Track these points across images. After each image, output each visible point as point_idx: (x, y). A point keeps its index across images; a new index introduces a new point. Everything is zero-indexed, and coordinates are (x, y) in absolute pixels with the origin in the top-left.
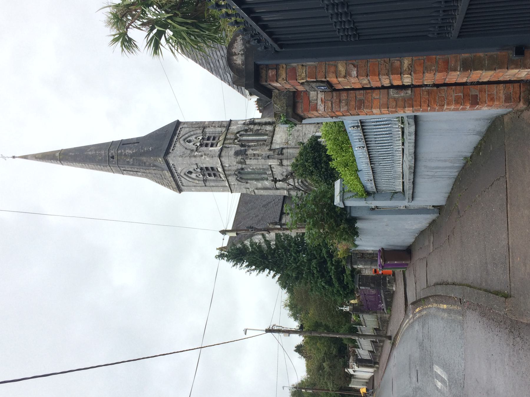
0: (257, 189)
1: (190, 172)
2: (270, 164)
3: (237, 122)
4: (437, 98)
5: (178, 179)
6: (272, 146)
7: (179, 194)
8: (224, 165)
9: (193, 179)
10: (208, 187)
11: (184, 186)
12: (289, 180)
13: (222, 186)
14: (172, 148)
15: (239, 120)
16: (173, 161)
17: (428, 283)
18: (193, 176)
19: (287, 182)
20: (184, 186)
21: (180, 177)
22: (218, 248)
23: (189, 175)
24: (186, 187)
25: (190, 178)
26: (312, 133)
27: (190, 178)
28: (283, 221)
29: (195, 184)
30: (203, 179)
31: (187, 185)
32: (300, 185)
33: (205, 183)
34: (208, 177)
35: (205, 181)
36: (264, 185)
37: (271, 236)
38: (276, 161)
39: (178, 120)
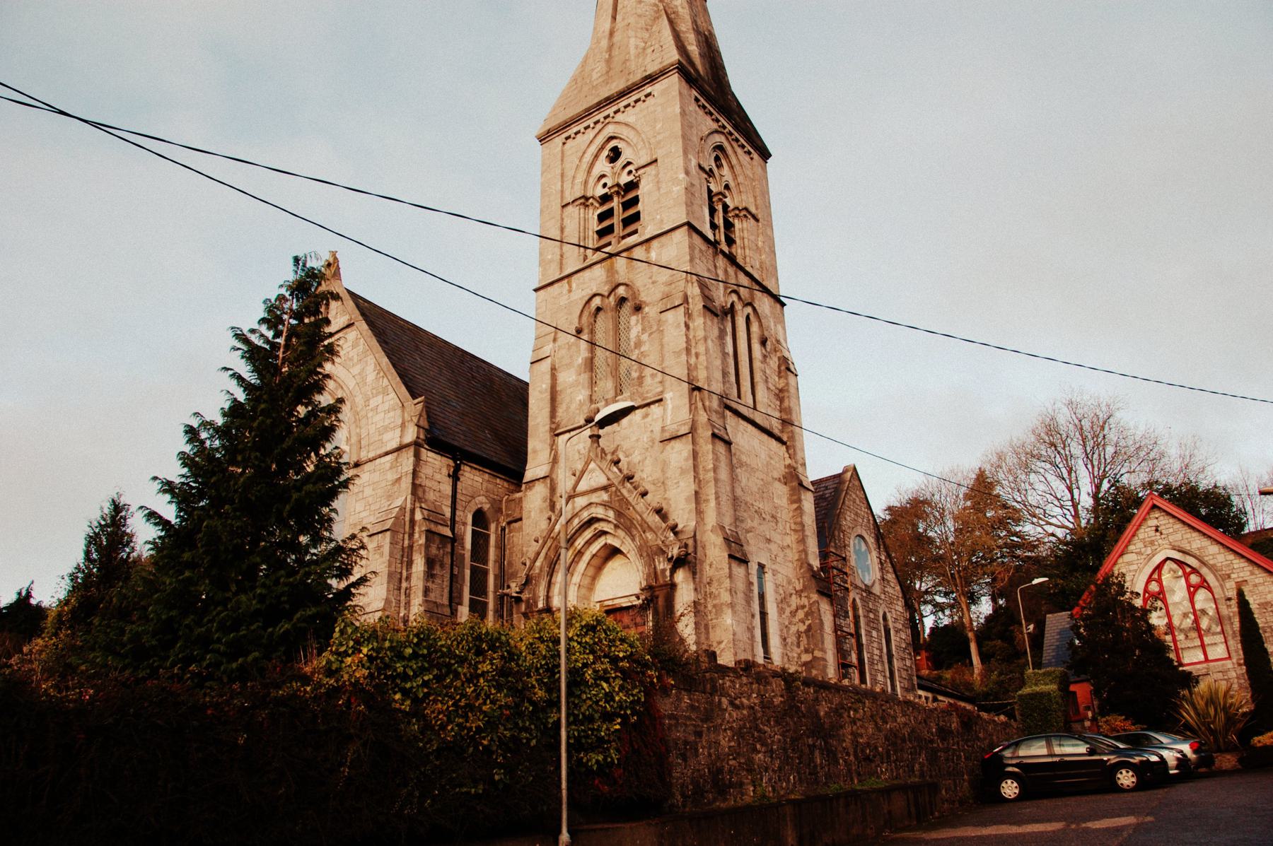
0: (553, 369)
1: (615, 154)
2: (668, 396)
3: (781, 320)
4: (340, 683)
5: (590, 122)
6: (690, 447)
7: (536, 134)
8: (655, 243)
9: (592, 165)
10: (560, 212)
11: (564, 144)
12: (598, 472)
13: (562, 256)
14: (703, 101)
15: (784, 328)
16: (664, 92)
17: (561, 412)
18: (602, 166)
19: (592, 465)
20: (564, 144)
21: (599, 126)
22: (337, 256)
23: (606, 153)
24: (559, 149)
25: (596, 156)
26: (773, 567)
27: (596, 156)
28: (430, 454)
29: (570, 173)
30: (589, 194)
31: (568, 153)
32: (569, 521)
33: (573, 202)
34: (599, 211)
35: (584, 201)
36: (569, 391)
37: (370, 415)
38: (685, 414)
39: (770, 155)
